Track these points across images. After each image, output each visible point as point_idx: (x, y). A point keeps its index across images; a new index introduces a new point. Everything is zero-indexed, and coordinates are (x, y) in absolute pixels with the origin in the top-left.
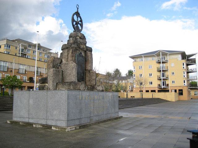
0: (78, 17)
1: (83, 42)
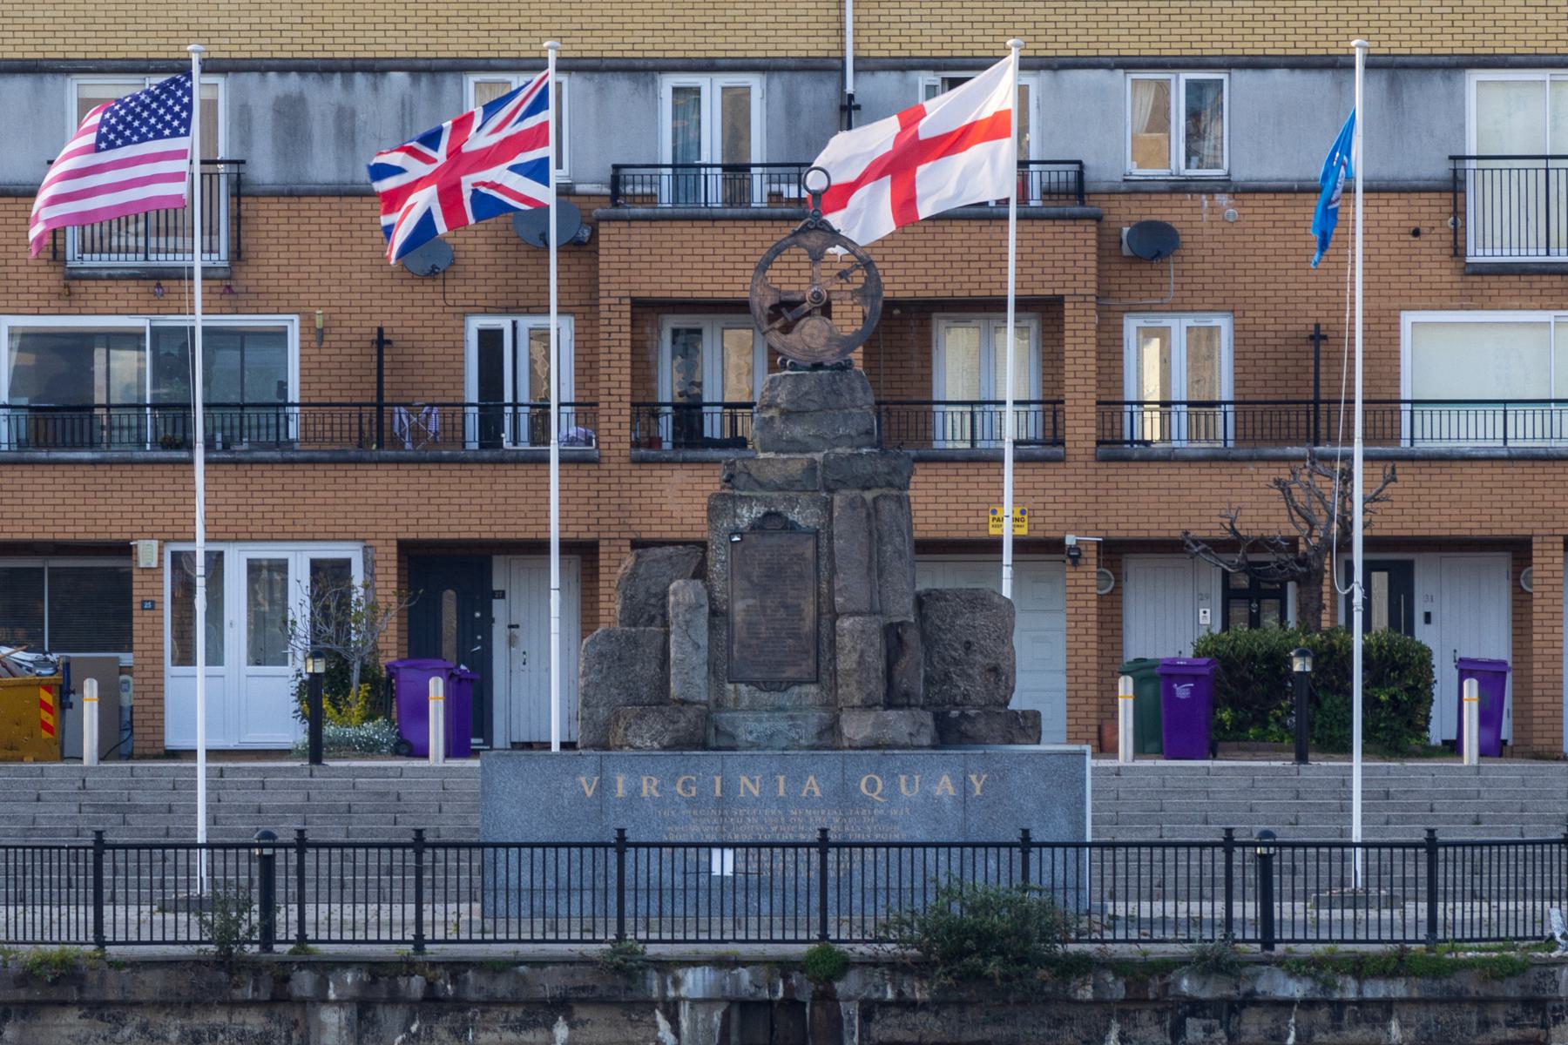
1: (815, 436)
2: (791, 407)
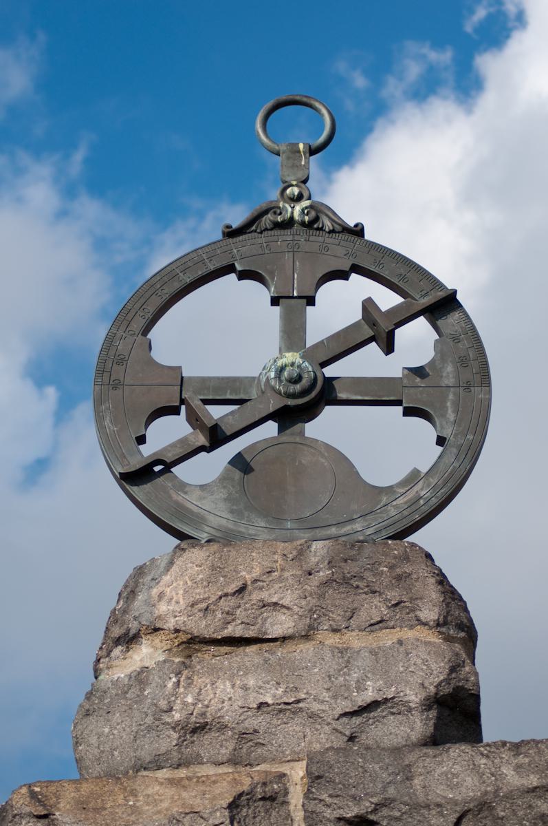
0: (294, 303)
2: (202, 626)
